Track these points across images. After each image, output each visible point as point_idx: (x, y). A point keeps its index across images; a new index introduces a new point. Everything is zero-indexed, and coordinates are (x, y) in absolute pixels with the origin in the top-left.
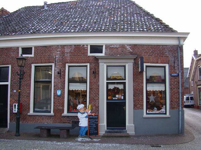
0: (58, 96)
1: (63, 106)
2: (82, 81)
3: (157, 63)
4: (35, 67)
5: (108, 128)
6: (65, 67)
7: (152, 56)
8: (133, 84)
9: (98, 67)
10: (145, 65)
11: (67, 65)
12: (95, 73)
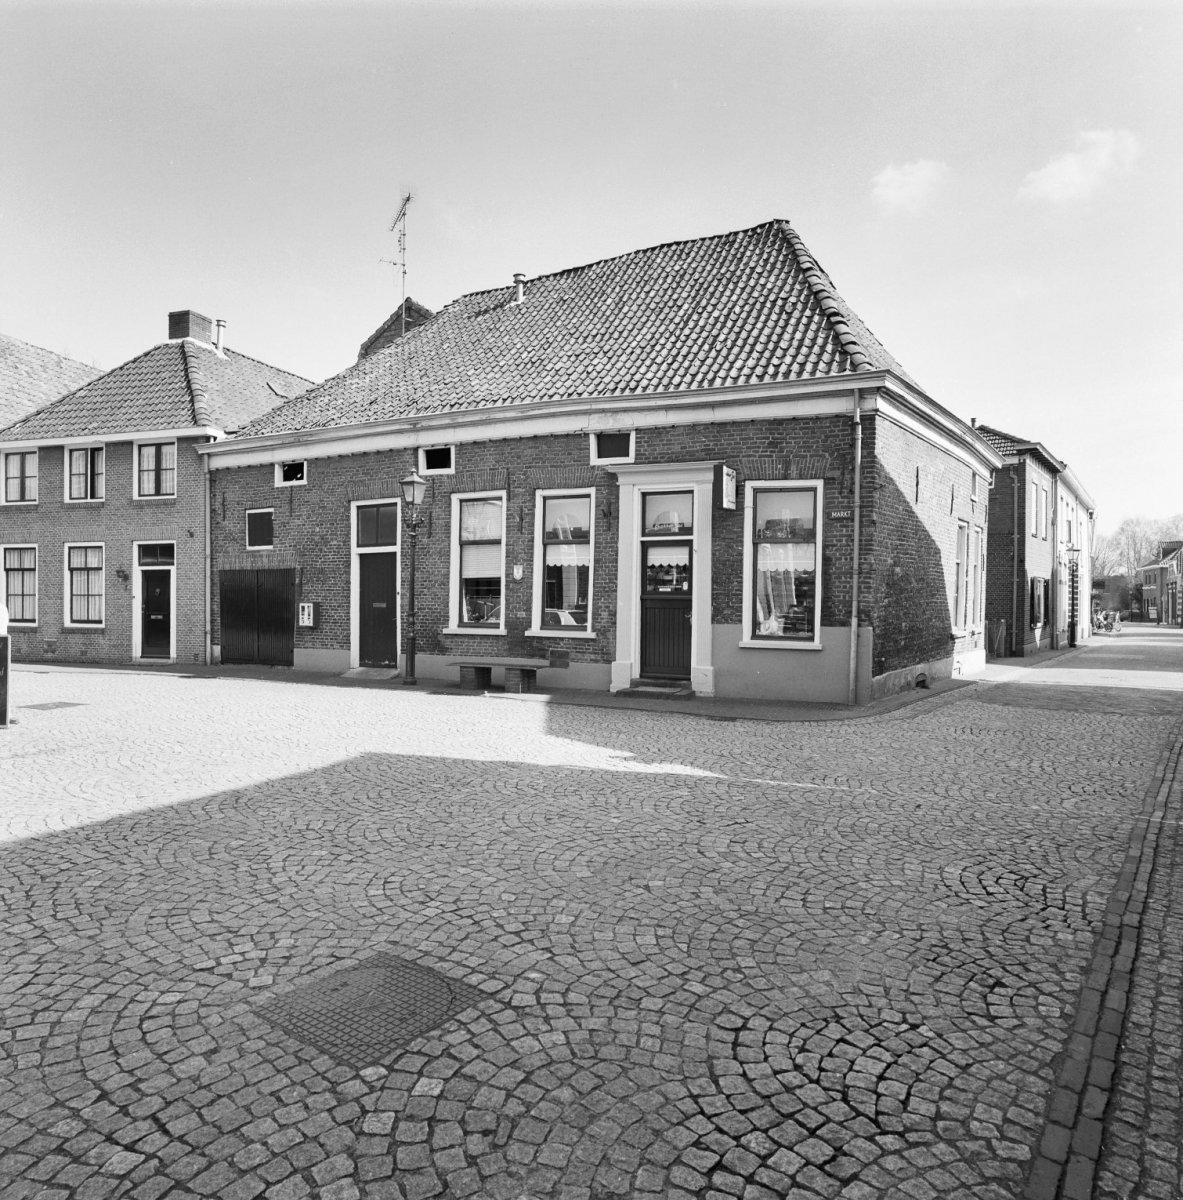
0: (515, 581)
1: (529, 610)
2: (580, 537)
3: (786, 477)
4: (359, 507)
5: (143, 561)
6: (348, 509)
7: (771, 456)
8: (713, 546)
9: (617, 498)
10: (749, 486)
11: (539, 494)
12: (609, 515)
